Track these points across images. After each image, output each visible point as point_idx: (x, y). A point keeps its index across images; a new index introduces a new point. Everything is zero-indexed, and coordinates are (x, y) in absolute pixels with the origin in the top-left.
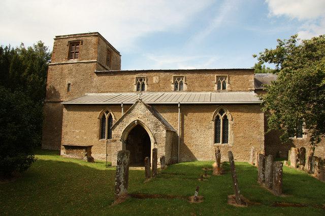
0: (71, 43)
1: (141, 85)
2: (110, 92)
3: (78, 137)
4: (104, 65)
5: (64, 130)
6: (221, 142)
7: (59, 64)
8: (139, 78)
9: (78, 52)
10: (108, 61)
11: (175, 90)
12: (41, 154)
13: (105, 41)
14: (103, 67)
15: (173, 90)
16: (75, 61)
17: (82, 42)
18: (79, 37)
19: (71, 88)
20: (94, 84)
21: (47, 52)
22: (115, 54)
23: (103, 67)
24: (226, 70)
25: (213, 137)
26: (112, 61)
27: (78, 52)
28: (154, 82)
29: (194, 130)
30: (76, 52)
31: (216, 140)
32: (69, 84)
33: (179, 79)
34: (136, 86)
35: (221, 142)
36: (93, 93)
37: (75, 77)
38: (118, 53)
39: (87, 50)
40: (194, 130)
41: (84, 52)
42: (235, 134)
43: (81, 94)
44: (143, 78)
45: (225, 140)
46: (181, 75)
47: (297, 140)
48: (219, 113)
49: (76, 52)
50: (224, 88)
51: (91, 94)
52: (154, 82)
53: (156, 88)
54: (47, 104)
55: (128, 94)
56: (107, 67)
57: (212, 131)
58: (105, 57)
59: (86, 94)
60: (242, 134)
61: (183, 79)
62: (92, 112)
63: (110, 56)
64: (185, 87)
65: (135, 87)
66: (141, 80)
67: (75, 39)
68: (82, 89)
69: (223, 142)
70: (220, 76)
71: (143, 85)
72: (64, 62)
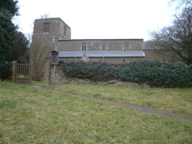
1: (84, 47)
2: (67, 51)
4: (63, 36)
7: (38, 35)
14: (62, 37)
22: (68, 29)
23: (62, 37)
28: (91, 45)
33: (104, 44)
38: (69, 28)
42: (52, 33)
46: (105, 42)
48: (123, 61)
52: (91, 45)
55: (77, 52)
56: (64, 37)
58: (63, 31)
62: (30, 59)
65: (81, 48)
66: (84, 44)
67: (46, 21)
70: (125, 43)
71: (85, 47)
72: (41, 34)
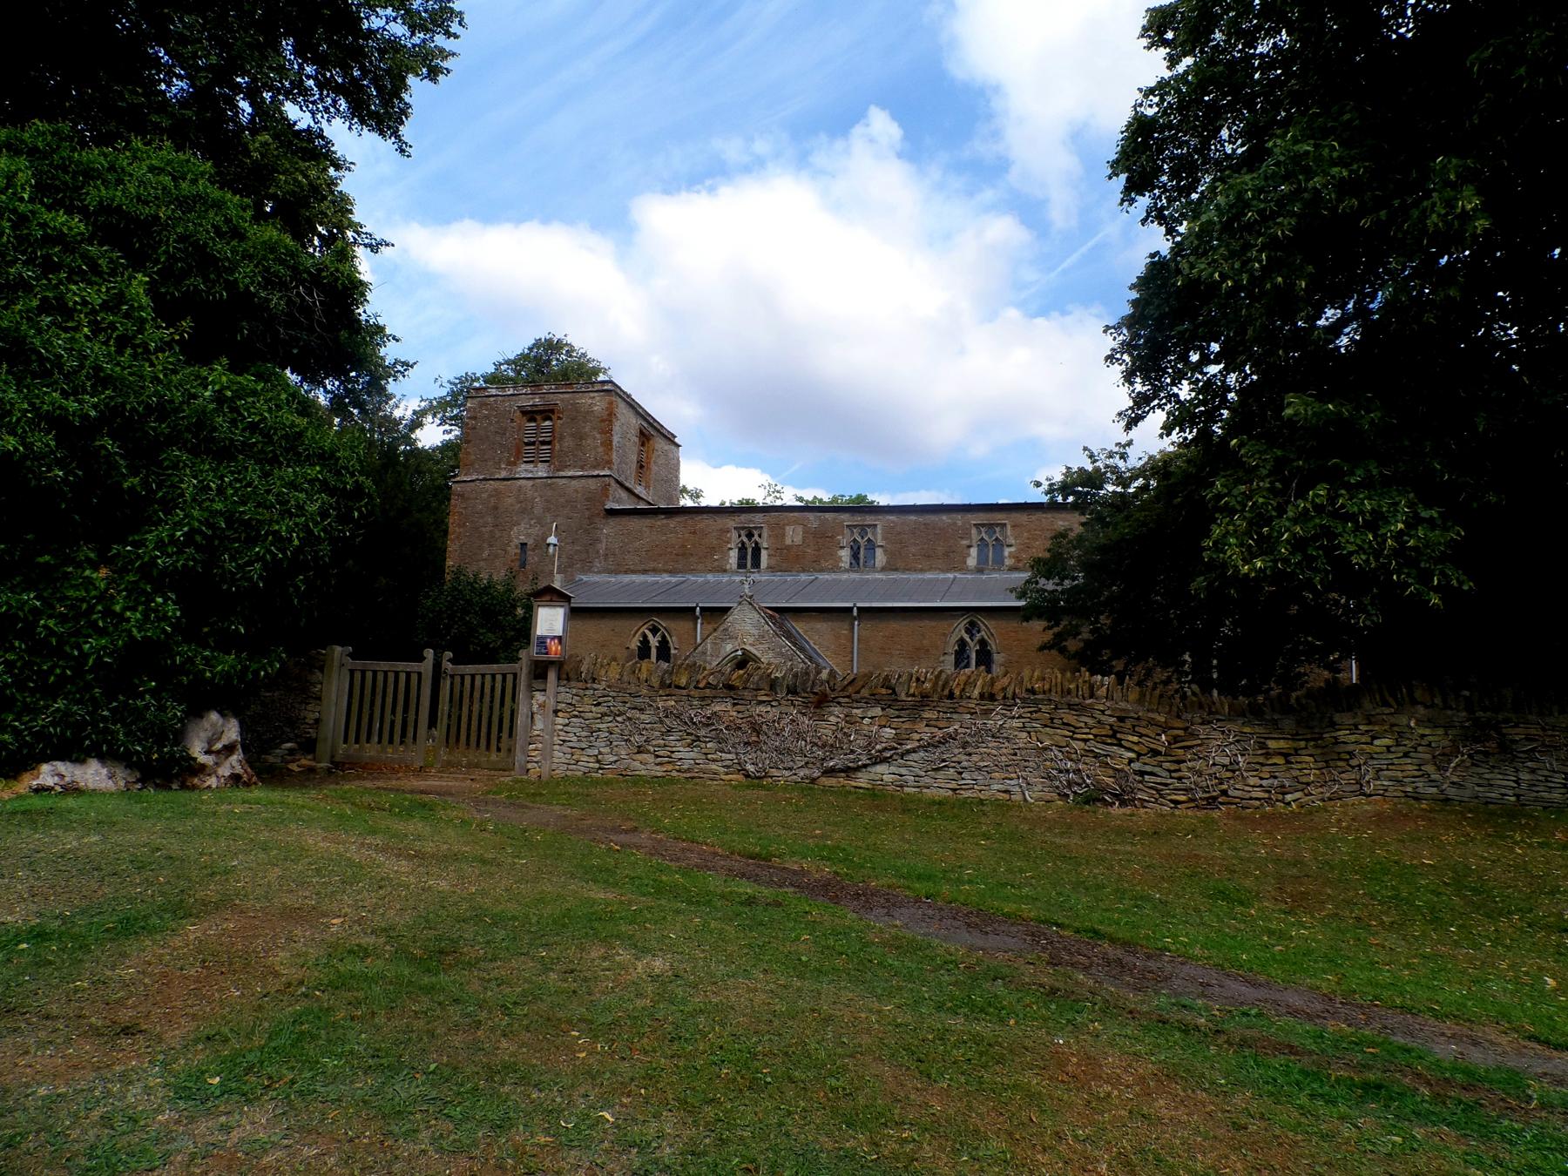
2: (655, 571)
8: (743, 528)
10: (642, 467)
12: (491, 212)
13: (633, 406)
14: (689, 656)
21: (397, 413)
22: (660, 444)
26: (654, 468)
32: (524, 545)
44: (755, 528)
52: (788, 541)
53: (789, 560)
55: (710, 577)
56: (639, 490)
58: (634, 458)
61: (874, 534)
64: (880, 558)
66: (750, 535)
71: (757, 551)
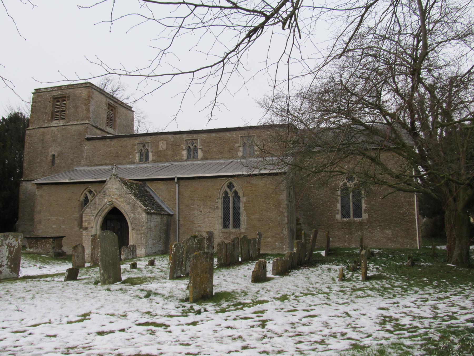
0: (54, 99)
3: (54, 226)
4: (103, 127)
5: (37, 217)
6: (231, 228)
9: (65, 111)
11: (189, 158)
14: (100, 129)
15: (184, 158)
16: (61, 123)
17: (69, 97)
18: (95, 89)
19: (57, 161)
20: (85, 155)
22: (121, 110)
23: (100, 129)
24: (254, 127)
25: (221, 221)
26: (118, 121)
27: (65, 111)
29: (196, 212)
30: (63, 111)
31: (225, 226)
34: (138, 155)
35: (351, 215)
36: (83, 166)
37: (60, 145)
38: (129, 108)
39: (76, 107)
40: (196, 212)
41: (72, 110)
43: (69, 168)
45: (237, 224)
47: (354, 222)
49: (63, 111)
50: (147, 159)
51: (82, 168)
54: (24, 183)
57: (220, 213)
59: (75, 168)
60: (257, 216)
63: (115, 114)
64: (200, 154)
66: (144, 146)
68: (70, 161)
69: (235, 227)
71: (147, 152)
72: (46, 125)
